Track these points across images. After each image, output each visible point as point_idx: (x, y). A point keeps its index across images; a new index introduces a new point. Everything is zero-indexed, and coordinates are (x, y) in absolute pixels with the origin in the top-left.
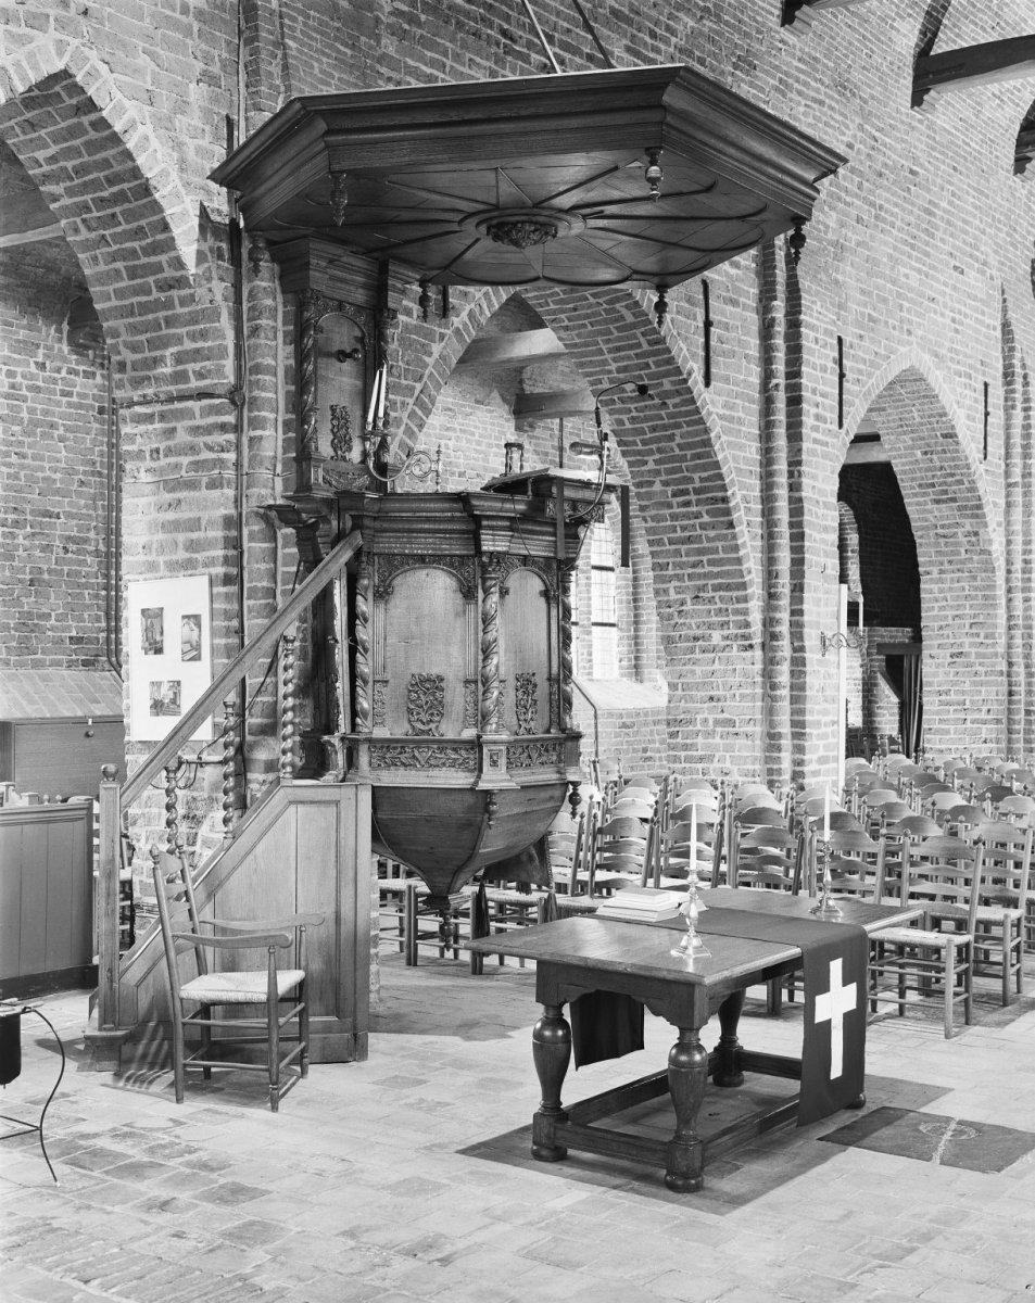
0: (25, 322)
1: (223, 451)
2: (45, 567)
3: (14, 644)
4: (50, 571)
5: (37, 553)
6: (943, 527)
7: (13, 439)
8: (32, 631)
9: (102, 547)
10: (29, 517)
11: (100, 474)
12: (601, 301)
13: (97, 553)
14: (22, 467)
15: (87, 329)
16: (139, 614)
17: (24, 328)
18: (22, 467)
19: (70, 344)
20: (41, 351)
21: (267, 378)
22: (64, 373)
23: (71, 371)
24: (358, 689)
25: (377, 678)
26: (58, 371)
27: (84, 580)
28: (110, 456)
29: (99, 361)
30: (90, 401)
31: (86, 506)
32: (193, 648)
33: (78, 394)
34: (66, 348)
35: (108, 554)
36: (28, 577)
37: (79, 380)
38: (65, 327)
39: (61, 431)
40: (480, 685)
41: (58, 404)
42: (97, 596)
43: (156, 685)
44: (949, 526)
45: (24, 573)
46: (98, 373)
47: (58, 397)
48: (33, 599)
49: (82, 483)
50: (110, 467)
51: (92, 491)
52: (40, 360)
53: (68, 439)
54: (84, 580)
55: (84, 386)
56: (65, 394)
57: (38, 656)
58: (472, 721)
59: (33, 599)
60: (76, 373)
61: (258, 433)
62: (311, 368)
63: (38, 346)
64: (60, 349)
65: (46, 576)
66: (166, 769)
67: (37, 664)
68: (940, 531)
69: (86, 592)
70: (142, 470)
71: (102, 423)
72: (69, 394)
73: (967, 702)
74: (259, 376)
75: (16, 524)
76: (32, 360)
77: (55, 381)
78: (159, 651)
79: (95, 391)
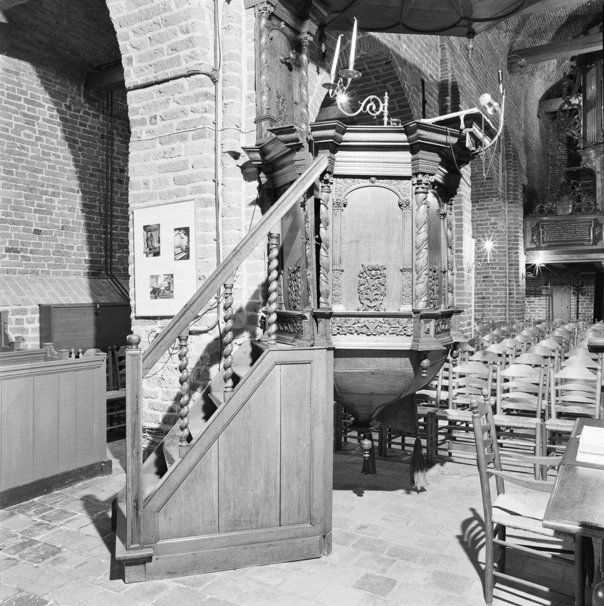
0: (59, 81)
1: (206, 112)
2: (71, 220)
3: (53, 262)
4: (73, 222)
5: (66, 212)
6: (480, 220)
7: (52, 146)
8: (63, 255)
9: (102, 211)
10: (61, 191)
11: (102, 171)
12: (379, 81)
13: (100, 214)
14: (57, 163)
15: (95, 88)
16: (142, 230)
17: (58, 84)
18: (57, 163)
19: (85, 98)
20: (68, 99)
21: (236, 62)
22: (81, 114)
23: (85, 113)
24: (321, 275)
25: (335, 268)
26: (78, 111)
27: (93, 228)
28: (107, 162)
29: (101, 109)
30: (96, 131)
31: (94, 188)
32: (183, 251)
33: (90, 126)
34: (83, 100)
35: (106, 215)
36: (61, 225)
37: (90, 118)
38: (82, 88)
39: (80, 145)
40: (414, 272)
41: (78, 130)
42: (100, 238)
43: (155, 277)
44: (485, 220)
45: (58, 222)
46: (101, 116)
47: (78, 126)
48: (63, 237)
49: (91, 175)
50: (107, 168)
51: (97, 180)
52: (68, 103)
53: (84, 150)
54: (93, 228)
55: (93, 122)
56: (81, 124)
57: (67, 269)
58: (407, 300)
59: (63, 237)
60: (89, 114)
61: (231, 100)
62: (263, 56)
63: (67, 96)
64: (80, 100)
65: (71, 225)
66: (179, 337)
67: (67, 274)
68: (479, 222)
69: (94, 235)
70: (144, 132)
71: (103, 143)
72: (85, 125)
73: (491, 298)
74: (231, 61)
75: (54, 194)
76: (63, 104)
77: (76, 117)
78: (157, 254)
79: (99, 126)
